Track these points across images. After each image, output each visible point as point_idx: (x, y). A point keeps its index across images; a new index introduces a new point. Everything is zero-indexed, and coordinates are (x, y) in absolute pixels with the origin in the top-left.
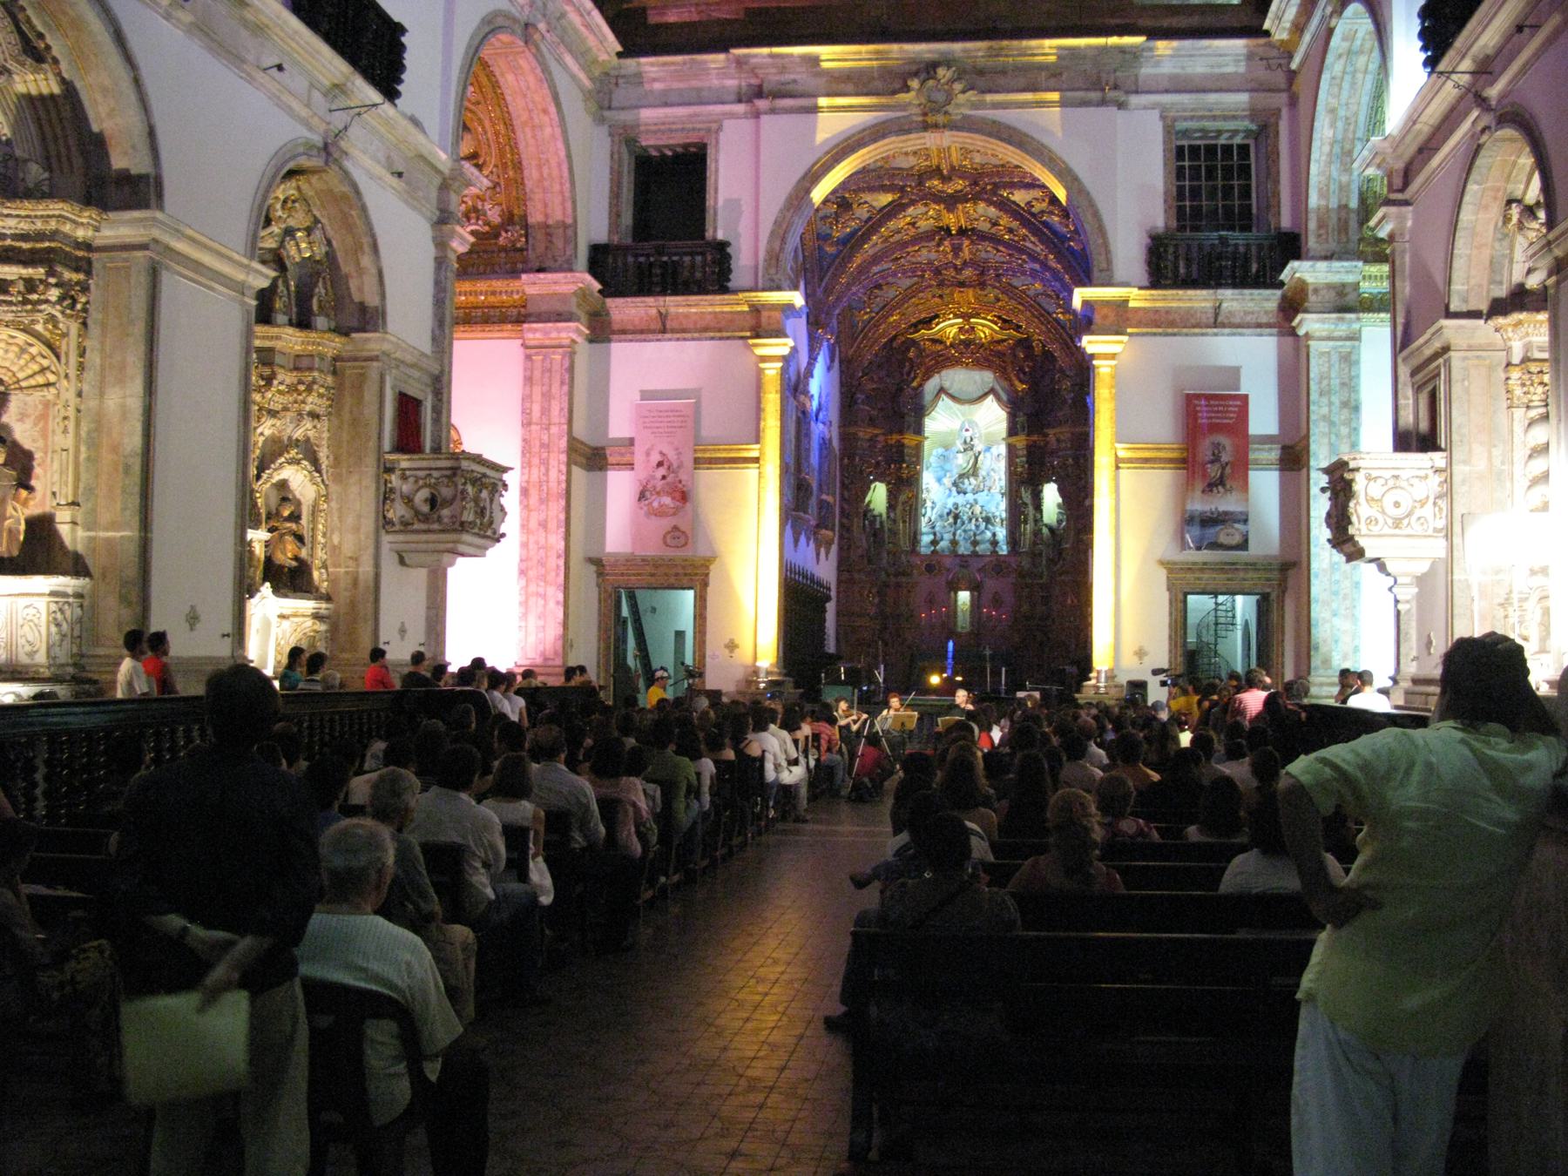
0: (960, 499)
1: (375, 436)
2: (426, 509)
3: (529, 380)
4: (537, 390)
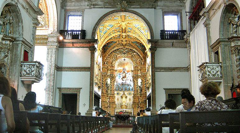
0: (123, 81)
4: (50, 55)
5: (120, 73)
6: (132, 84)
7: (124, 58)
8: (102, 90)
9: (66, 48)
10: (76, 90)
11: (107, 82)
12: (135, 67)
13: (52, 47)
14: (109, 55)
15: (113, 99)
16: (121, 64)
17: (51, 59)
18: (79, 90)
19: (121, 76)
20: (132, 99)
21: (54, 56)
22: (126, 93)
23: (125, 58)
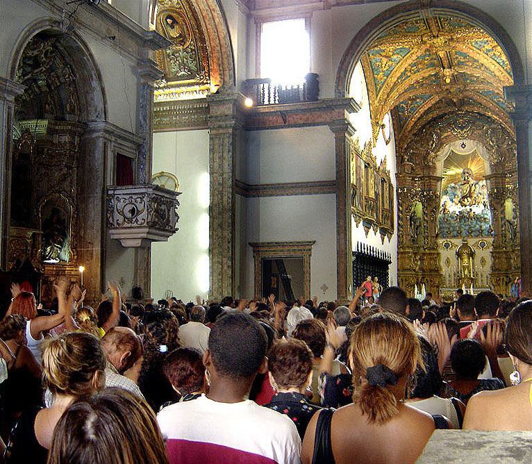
1: (102, 178)
2: (129, 215)
3: (212, 150)
4: (217, 156)
5: (453, 185)
6: (489, 215)
7: (461, 142)
8: (399, 236)
9: (264, 131)
10: (301, 248)
11: (414, 212)
12: (494, 167)
13: (221, 131)
14: (415, 135)
15: (432, 262)
16: (452, 160)
17: (221, 166)
18: (308, 247)
19: (459, 193)
20: (489, 261)
21: (228, 156)
22: (471, 242)
23: (465, 142)
